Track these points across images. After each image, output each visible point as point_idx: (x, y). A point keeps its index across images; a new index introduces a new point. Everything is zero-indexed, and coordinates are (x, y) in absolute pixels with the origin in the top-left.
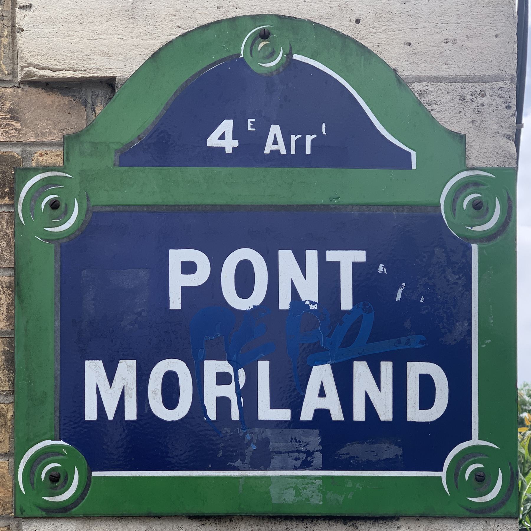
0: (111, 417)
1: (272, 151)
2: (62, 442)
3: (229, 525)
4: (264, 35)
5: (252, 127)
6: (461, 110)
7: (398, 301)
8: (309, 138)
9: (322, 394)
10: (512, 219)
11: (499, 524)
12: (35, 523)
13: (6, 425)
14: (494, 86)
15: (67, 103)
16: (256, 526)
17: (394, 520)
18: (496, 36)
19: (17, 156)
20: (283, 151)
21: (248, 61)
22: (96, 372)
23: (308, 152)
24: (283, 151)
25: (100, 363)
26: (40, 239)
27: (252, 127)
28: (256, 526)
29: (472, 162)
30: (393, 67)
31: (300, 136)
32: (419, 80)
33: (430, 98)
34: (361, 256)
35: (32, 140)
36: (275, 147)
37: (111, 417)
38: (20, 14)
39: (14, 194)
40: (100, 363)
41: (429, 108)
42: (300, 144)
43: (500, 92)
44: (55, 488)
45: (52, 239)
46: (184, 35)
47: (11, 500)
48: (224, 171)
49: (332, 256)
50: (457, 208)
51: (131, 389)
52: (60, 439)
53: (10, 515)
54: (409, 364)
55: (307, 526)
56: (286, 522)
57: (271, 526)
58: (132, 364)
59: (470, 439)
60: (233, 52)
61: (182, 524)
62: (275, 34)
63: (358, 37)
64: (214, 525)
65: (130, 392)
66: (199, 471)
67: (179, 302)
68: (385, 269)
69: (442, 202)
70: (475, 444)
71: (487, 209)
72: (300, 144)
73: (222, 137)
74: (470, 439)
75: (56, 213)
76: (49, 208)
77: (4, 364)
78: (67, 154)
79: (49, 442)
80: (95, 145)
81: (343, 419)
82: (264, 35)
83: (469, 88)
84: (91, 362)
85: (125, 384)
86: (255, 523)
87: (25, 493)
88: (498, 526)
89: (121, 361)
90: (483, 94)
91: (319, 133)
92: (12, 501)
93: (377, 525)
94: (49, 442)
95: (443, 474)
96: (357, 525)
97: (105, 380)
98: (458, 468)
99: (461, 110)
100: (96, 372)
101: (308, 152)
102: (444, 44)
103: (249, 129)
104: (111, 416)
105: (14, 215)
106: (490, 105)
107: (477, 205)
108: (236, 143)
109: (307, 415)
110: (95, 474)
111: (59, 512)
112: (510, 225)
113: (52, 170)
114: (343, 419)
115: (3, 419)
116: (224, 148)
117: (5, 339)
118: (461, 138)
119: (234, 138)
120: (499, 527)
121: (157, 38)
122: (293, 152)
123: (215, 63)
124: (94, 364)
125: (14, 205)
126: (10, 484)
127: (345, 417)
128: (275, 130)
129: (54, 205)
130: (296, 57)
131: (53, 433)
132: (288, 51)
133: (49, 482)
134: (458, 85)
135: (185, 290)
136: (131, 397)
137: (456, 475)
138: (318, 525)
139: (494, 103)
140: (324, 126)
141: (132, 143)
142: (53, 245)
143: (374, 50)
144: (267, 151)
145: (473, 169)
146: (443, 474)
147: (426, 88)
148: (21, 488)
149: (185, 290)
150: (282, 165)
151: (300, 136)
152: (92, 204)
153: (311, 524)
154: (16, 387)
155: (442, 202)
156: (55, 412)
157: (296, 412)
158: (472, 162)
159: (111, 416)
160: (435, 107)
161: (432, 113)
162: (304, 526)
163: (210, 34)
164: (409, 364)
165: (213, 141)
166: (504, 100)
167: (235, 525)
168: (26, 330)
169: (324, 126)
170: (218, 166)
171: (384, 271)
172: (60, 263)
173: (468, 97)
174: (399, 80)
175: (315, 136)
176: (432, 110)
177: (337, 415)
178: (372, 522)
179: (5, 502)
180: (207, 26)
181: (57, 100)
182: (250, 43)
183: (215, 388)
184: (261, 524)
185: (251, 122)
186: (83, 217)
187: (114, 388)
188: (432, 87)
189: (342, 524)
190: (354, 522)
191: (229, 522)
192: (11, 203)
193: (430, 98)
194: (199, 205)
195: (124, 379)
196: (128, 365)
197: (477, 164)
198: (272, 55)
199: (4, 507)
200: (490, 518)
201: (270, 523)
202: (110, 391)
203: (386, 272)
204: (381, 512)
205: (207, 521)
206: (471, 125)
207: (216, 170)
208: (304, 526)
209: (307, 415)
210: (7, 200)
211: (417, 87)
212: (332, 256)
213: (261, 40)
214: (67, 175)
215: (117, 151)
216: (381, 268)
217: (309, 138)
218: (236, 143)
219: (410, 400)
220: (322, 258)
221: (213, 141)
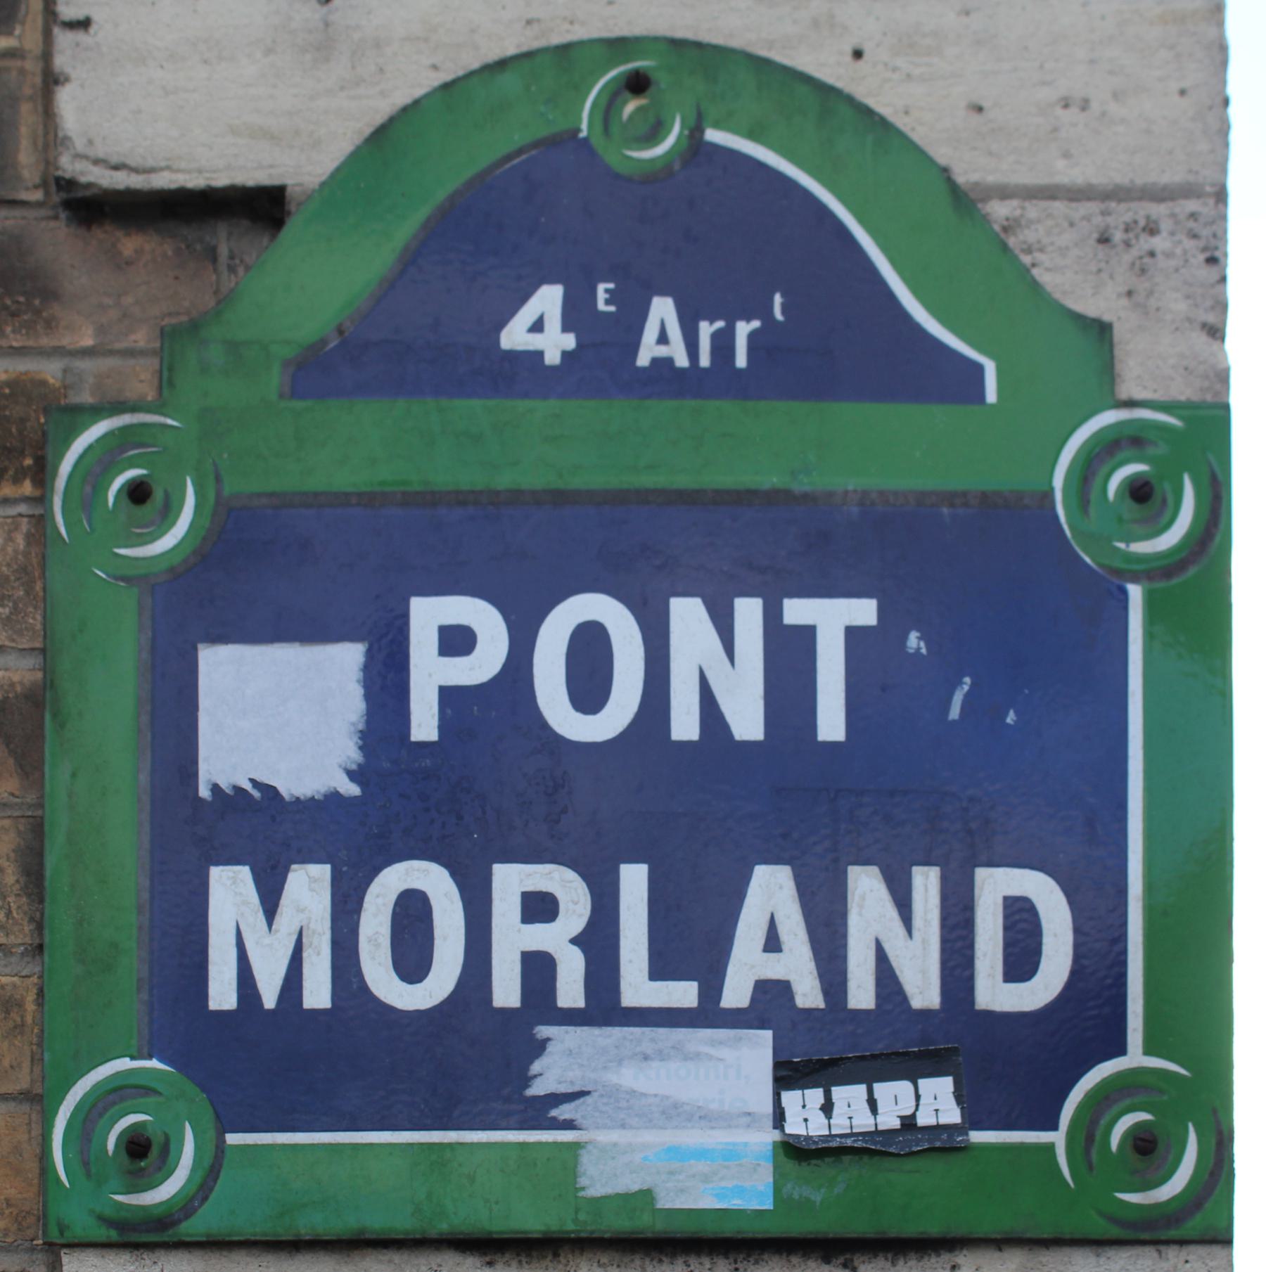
0: (269, 1001)
1: (656, 362)
2: (154, 1063)
3: (550, 1264)
4: (638, 84)
5: (608, 302)
6: (1103, 265)
7: (954, 721)
8: (743, 330)
9: (773, 943)
10: (1222, 526)
11: (1188, 1258)
12: (92, 1258)
13: (23, 1025)
14: (1177, 210)
15: (170, 253)
16: (615, 1266)
17: (942, 1252)
18: (1182, 92)
19: (51, 381)
20: (682, 361)
21: (598, 142)
22: (236, 893)
23: (741, 361)
24: (682, 361)
25: (244, 872)
26: (104, 576)
27: (608, 302)
28: (615, 1266)
29: (1129, 388)
30: (942, 161)
31: (720, 324)
32: (1004, 193)
33: (1029, 235)
34: (864, 612)
35: (88, 341)
36: (662, 351)
37: (269, 1001)
38: (63, 39)
39: (42, 473)
40: (244, 872)
41: (1026, 259)
42: (723, 343)
43: (1191, 224)
44: (140, 1173)
45: (134, 577)
46: (446, 87)
47: (36, 1207)
48: (540, 409)
49: (797, 611)
50: (1094, 496)
51: (319, 934)
52: (150, 1057)
53: (35, 1242)
54: (981, 874)
55: (737, 1266)
56: (688, 1258)
57: (651, 1266)
58: (321, 872)
59: (1121, 1050)
60: (562, 125)
61: (439, 1260)
62: (662, 80)
63: (862, 93)
64: (514, 1264)
65: (315, 942)
66: (479, 1132)
67: (435, 722)
68: (922, 644)
69: (1058, 481)
70: (1134, 1065)
71: (1164, 501)
72: (723, 343)
73: (538, 327)
74: (1121, 1050)
75: (148, 510)
76: (125, 501)
77: (17, 881)
78: (171, 369)
79: (124, 1064)
80: (233, 347)
81: (822, 1005)
82: (638, 84)
83: (1124, 213)
84: (223, 871)
85: (304, 923)
86: (614, 1260)
87: (68, 1186)
88: (1187, 1262)
89: (294, 867)
90: (1152, 229)
91: (767, 315)
92: (39, 1209)
93: (901, 1262)
94: (124, 1064)
95: (1057, 1138)
96: (856, 1263)
97: (256, 913)
98: (1094, 1122)
99: (1103, 265)
100: (236, 893)
101: (741, 361)
102: (1059, 111)
103: (601, 306)
104: (269, 999)
105: (42, 522)
106: (1169, 255)
107: (1139, 491)
108: (570, 341)
109: (736, 993)
110: (232, 1139)
111: (148, 1231)
112: (1218, 539)
113: (134, 409)
114: (822, 1005)
115: (17, 1013)
116: (539, 355)
117: (23, 820)
118: (1102, 330)
119: (566, 328)
120: (1188, 1265)
121: (383, 94)
122: (705, 361)
123: (520, 152)
124: (231, 874)
125: (42, 499)
126: (32, 1166)
127: (826, 1001)
128: (663, 310)
129: (138, 493)
130: (713, 135)
131: (134, 1042)
132: (692, 121)
133: (124, 1158)
134: (1093, 207)
135: (449, 696)
136: (318, 954)
137: (1090, 1139)
138: (764, 1264)
139: (1178, 251)
140: (778, 299)
141: (323, 342)
142: (135, 590)
143: (900, 122)
144: (643, 360)
145: (1131, 404)
146: (1057, 1138)
147: (1018, 212)
148: (60, 1173)
149: (449, 696)
150: (679, 394)
151: (720, 324)
152: (227, 491)
153: (745, 1262)
154: (46, 932)
155: (1058, 481)
156: (139, 990)
157: (712, 986)
158: (1129, 388)
159: (269, 999)
160: (1039, 256)
161: (1035, 272)
162: (730, 1268)
163: (509, 82)
164: (981, 874)
165: (515, 336)
166: (1202, 243)
167: (566, 1265)
168: (70, 796)
169: (778, 299)
170: (526, 395)
171: (919, 649)
172: (150, 634)
173: (1118, 236)
174: (955, 190)
175: (756, 324)
176: (1034, 265)
177: (808, 994)
178: (890, 1256)
179: (23, 1211)
180: (502, 65)
181: (147, 247)
182: (603, 102)
183: (519, 931)
184: (626, 1263)
185: (607, 291)
186: (206, 522)
187: (277, 931)
188: (1033, 210)
189: (819, 1261)
190: (848, 1256)
191: (550, 1257)
192: (37, 493)
193: (1029, 235)
194: (481, 492)
195: (302, 911)
196: (312, 875)
197: (1139, 395)
198: (654, 134)
199: (20, 1224)
200: (1168, 1242)
201: (647, 1261)
202: (268, 940)
203: (924, 651)
204: (911, 1229)
205: (500, 1255)
206: (1124, 302)
207: (522, 405)
208: (730, 1268)
209: (736, 993)
210: (27, 488)
211: (999, 210)
212: (797, 611)
213: (627, 94)
214: (170, 422)
215: (286, 364)
216: (913, 641)
217: (743, 330)
218: (570, 341)
219: (982, 958)
220: (772, 616)
221: (515, 336)
